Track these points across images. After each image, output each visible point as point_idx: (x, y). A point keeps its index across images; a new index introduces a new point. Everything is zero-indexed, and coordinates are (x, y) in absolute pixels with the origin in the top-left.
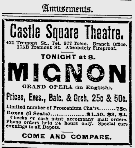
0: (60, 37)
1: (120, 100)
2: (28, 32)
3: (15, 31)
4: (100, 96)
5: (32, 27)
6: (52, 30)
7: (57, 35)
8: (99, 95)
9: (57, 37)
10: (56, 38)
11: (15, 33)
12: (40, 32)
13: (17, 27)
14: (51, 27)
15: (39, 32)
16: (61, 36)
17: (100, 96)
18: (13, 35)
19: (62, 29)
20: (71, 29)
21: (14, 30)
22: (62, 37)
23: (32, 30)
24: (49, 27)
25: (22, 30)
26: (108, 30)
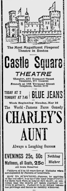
0: (47, 67)
1: (39, 157)
2: (19, 63)
3: (9, 63)
4: (30, 155)
5: (22, 58)
6: (39, 61)
7: (44, 65)
8: (30, 154)
9: (44, 67)
10: (43, 68)
11: (9, 64)
12: (29, 62)
13: (10, 59)
14: (39, 59)
15: (28, 63)
16: (47, 66)
17: (30, 155)
18: (7, 65)
19: (48, 60)
20: (56, 60)
21: (8, 62)
22: (48, 67)
23: (22, 61)
24: (37, 59)
25: (15, 61)
26: (20, 59)
